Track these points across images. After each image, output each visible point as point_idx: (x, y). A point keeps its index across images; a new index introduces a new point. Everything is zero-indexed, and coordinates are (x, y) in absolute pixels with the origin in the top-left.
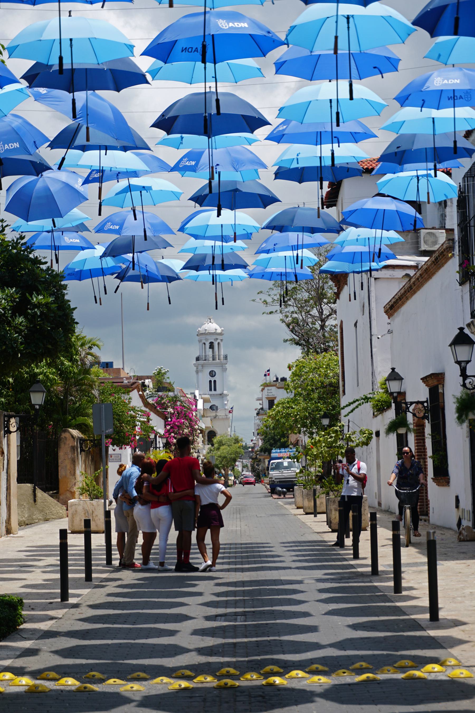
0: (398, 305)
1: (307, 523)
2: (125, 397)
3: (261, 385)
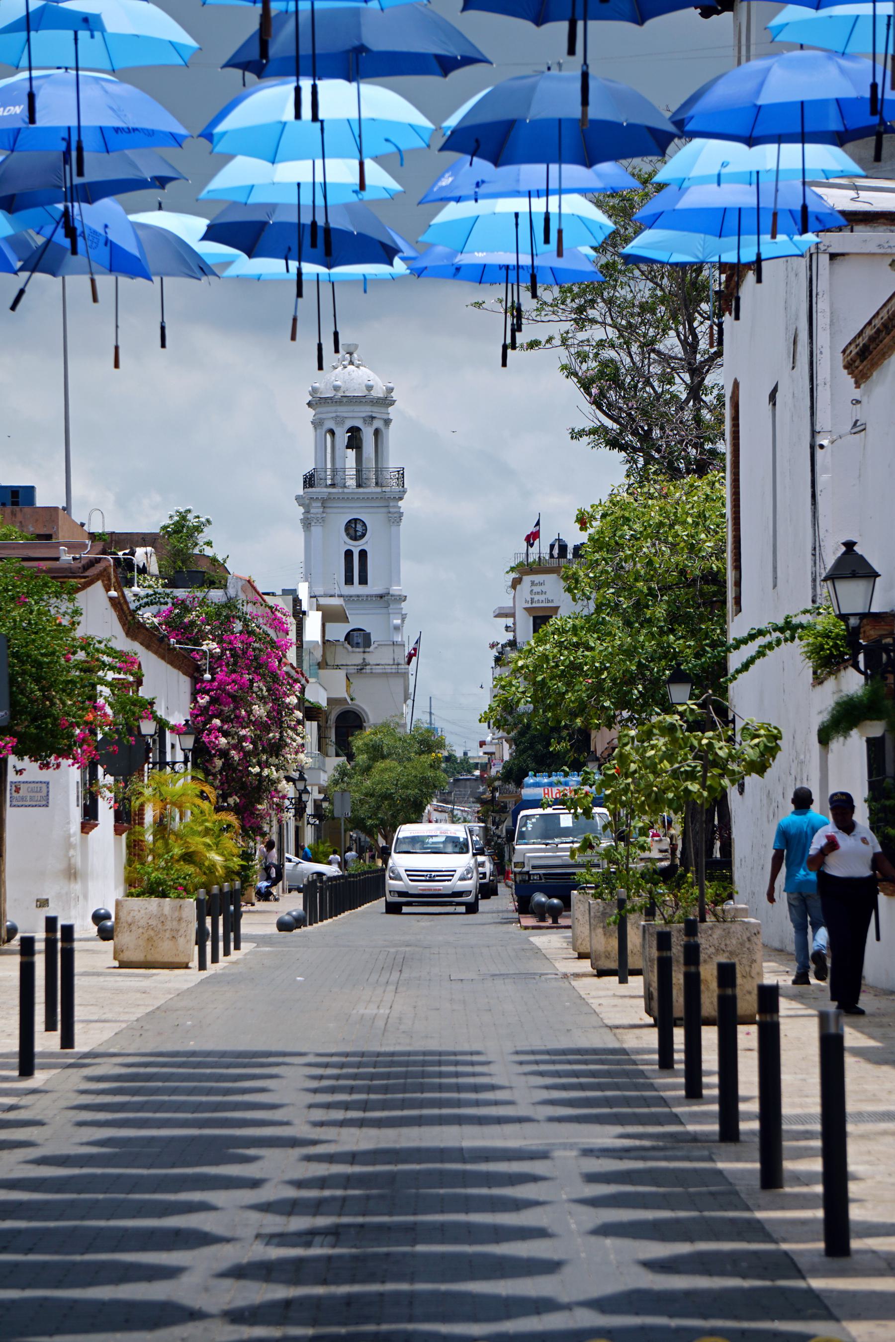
0: (881, 346)
1: (590, 1001)
2: (59, 608)
3: (512, 569)
